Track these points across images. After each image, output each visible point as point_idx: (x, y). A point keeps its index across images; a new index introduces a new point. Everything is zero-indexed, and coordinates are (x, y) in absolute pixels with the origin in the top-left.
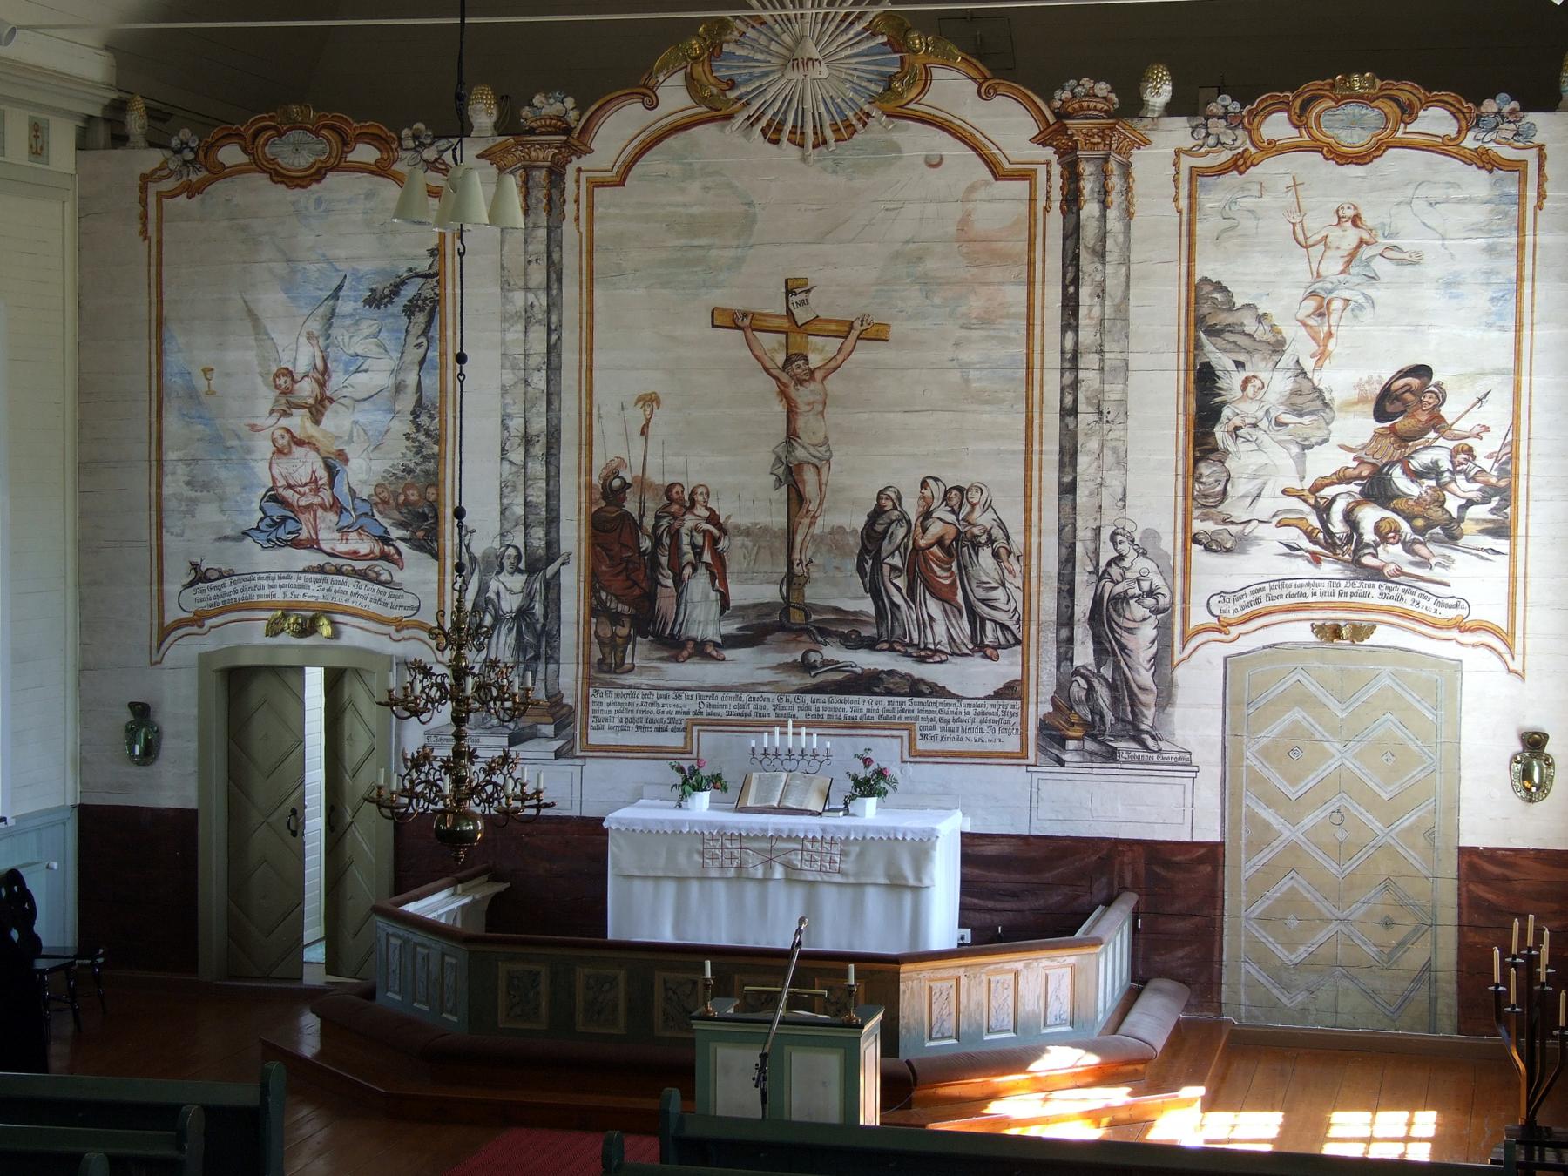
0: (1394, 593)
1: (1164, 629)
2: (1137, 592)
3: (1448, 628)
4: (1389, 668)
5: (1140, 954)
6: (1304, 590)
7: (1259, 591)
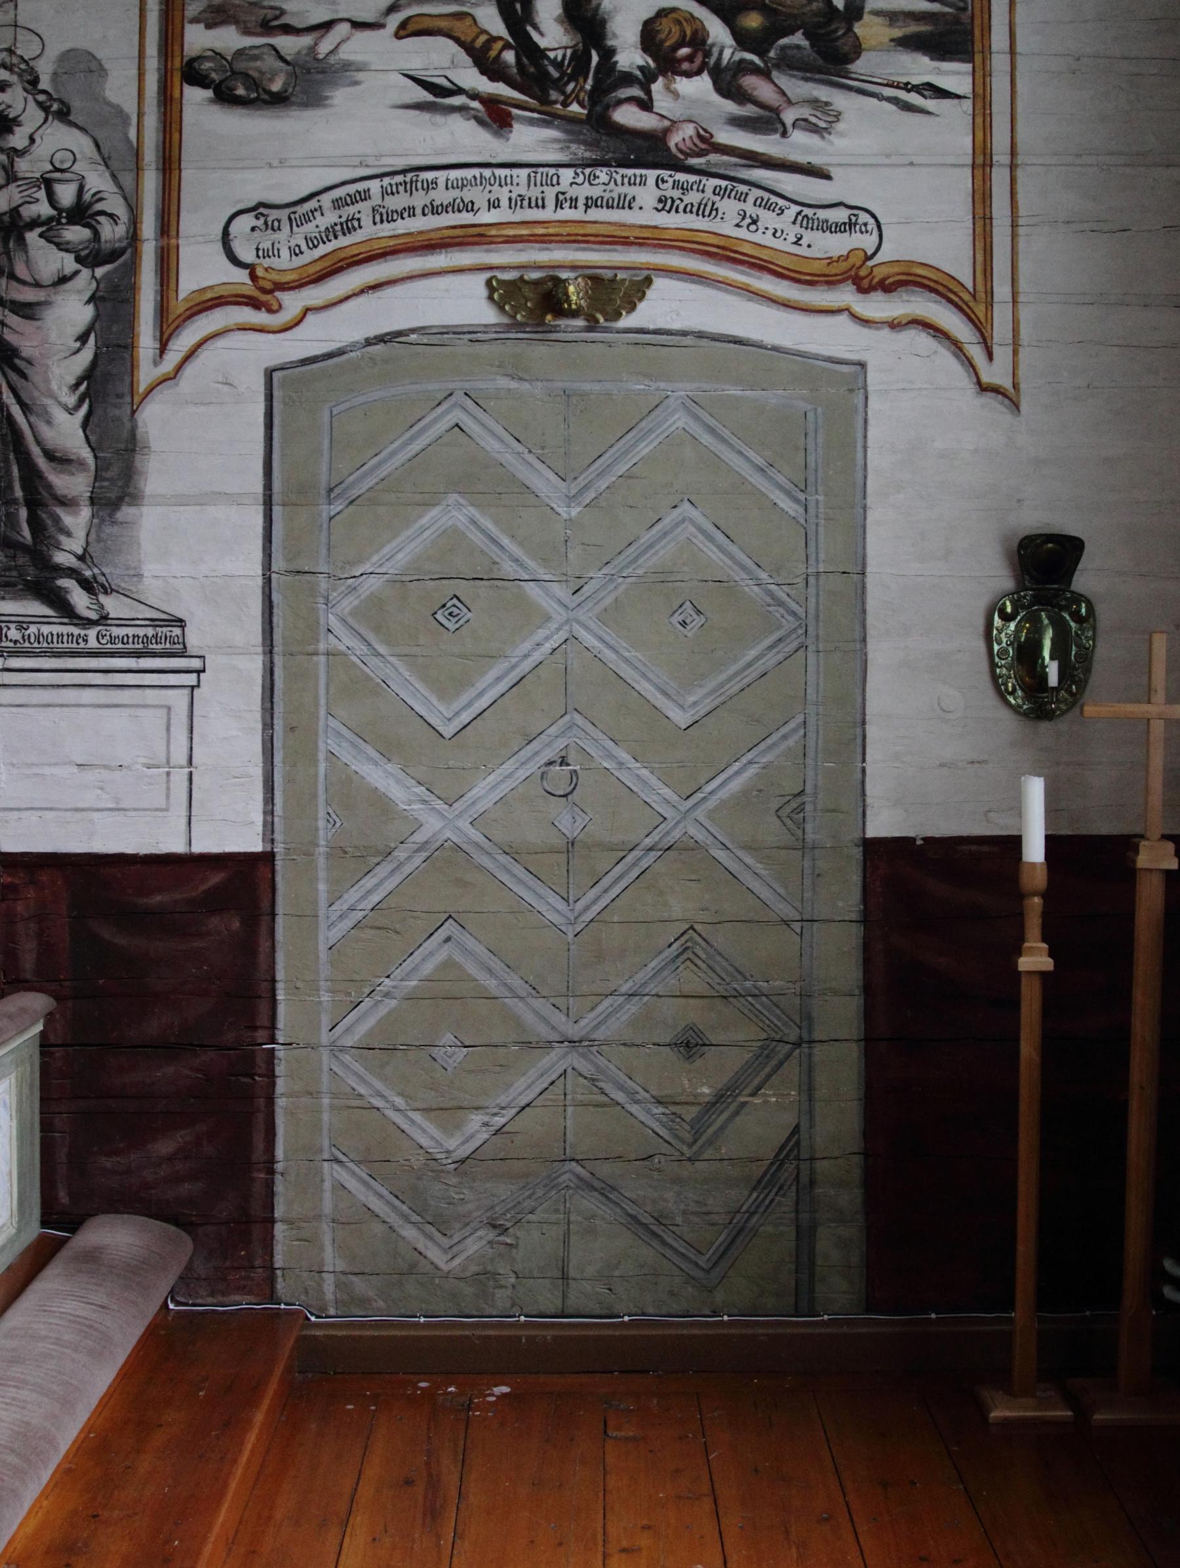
0: (693, 197)
1: (113, 304)
2: (44, 209)
3: (830, 281)
4: (682, 390)
5: (62, 1155)
6: (468, 195)
7: (353, 199)
